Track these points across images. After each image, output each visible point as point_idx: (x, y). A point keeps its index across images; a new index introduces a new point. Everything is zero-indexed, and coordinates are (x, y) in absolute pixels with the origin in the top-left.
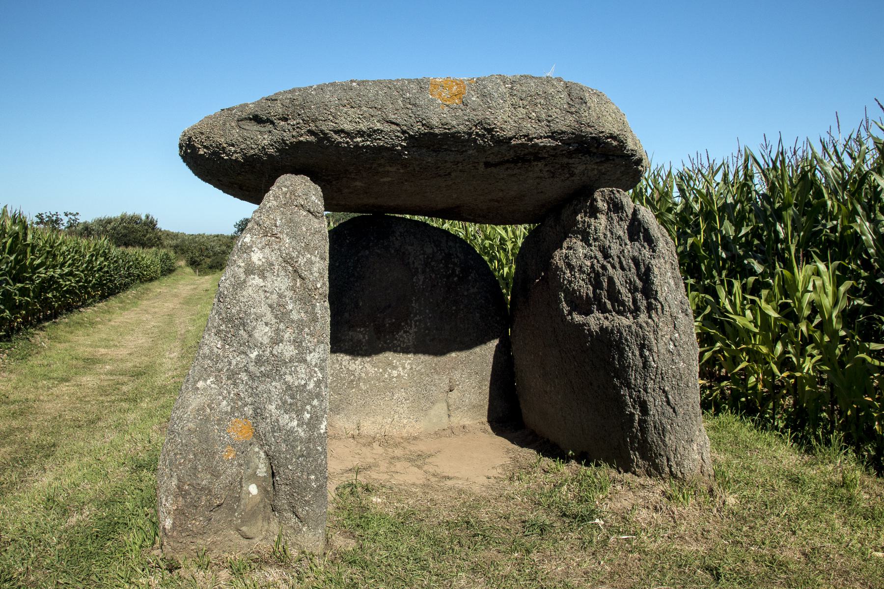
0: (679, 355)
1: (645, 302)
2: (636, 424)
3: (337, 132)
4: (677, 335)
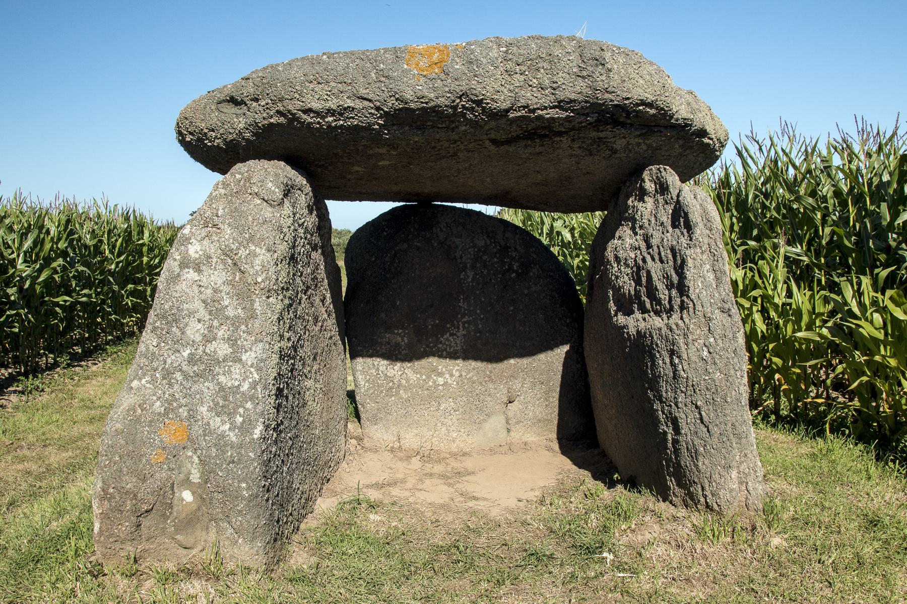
0: (715, 364)
1: (679, 300)
2: (670, 445)
3: (308, 111)
4: (712, 340)
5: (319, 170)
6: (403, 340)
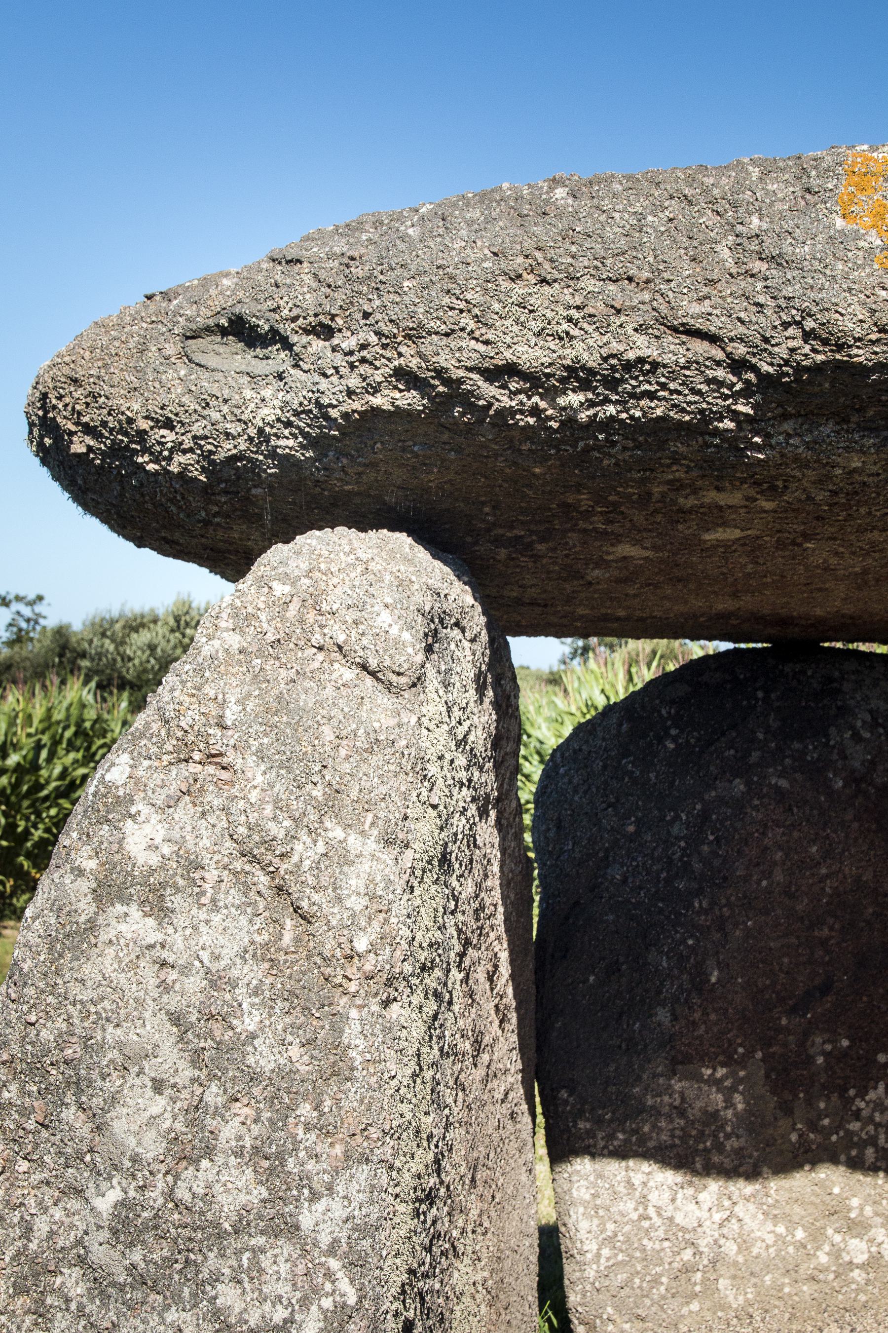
3: (498, 374)
5: (503, 553)
6: (729, 1103)
